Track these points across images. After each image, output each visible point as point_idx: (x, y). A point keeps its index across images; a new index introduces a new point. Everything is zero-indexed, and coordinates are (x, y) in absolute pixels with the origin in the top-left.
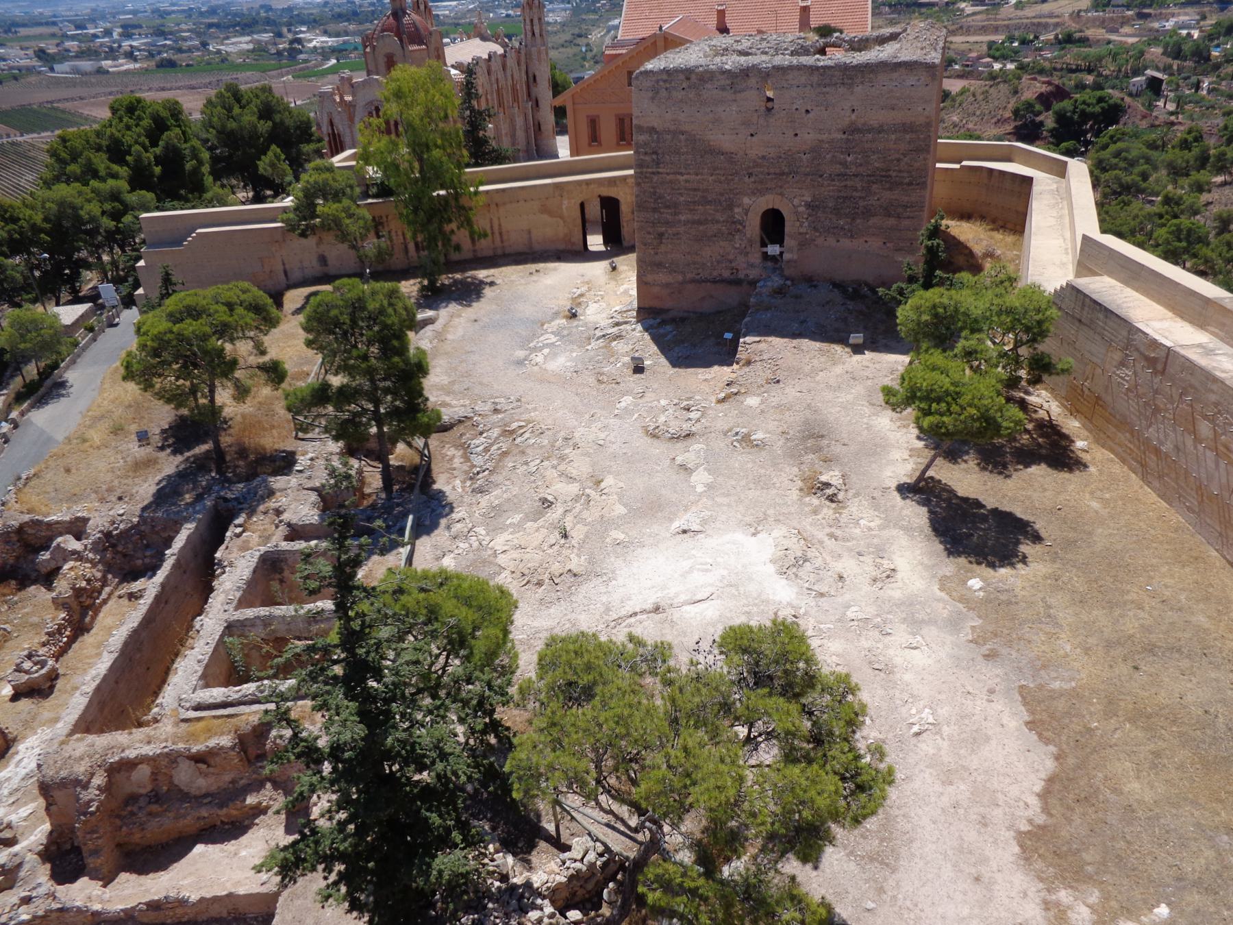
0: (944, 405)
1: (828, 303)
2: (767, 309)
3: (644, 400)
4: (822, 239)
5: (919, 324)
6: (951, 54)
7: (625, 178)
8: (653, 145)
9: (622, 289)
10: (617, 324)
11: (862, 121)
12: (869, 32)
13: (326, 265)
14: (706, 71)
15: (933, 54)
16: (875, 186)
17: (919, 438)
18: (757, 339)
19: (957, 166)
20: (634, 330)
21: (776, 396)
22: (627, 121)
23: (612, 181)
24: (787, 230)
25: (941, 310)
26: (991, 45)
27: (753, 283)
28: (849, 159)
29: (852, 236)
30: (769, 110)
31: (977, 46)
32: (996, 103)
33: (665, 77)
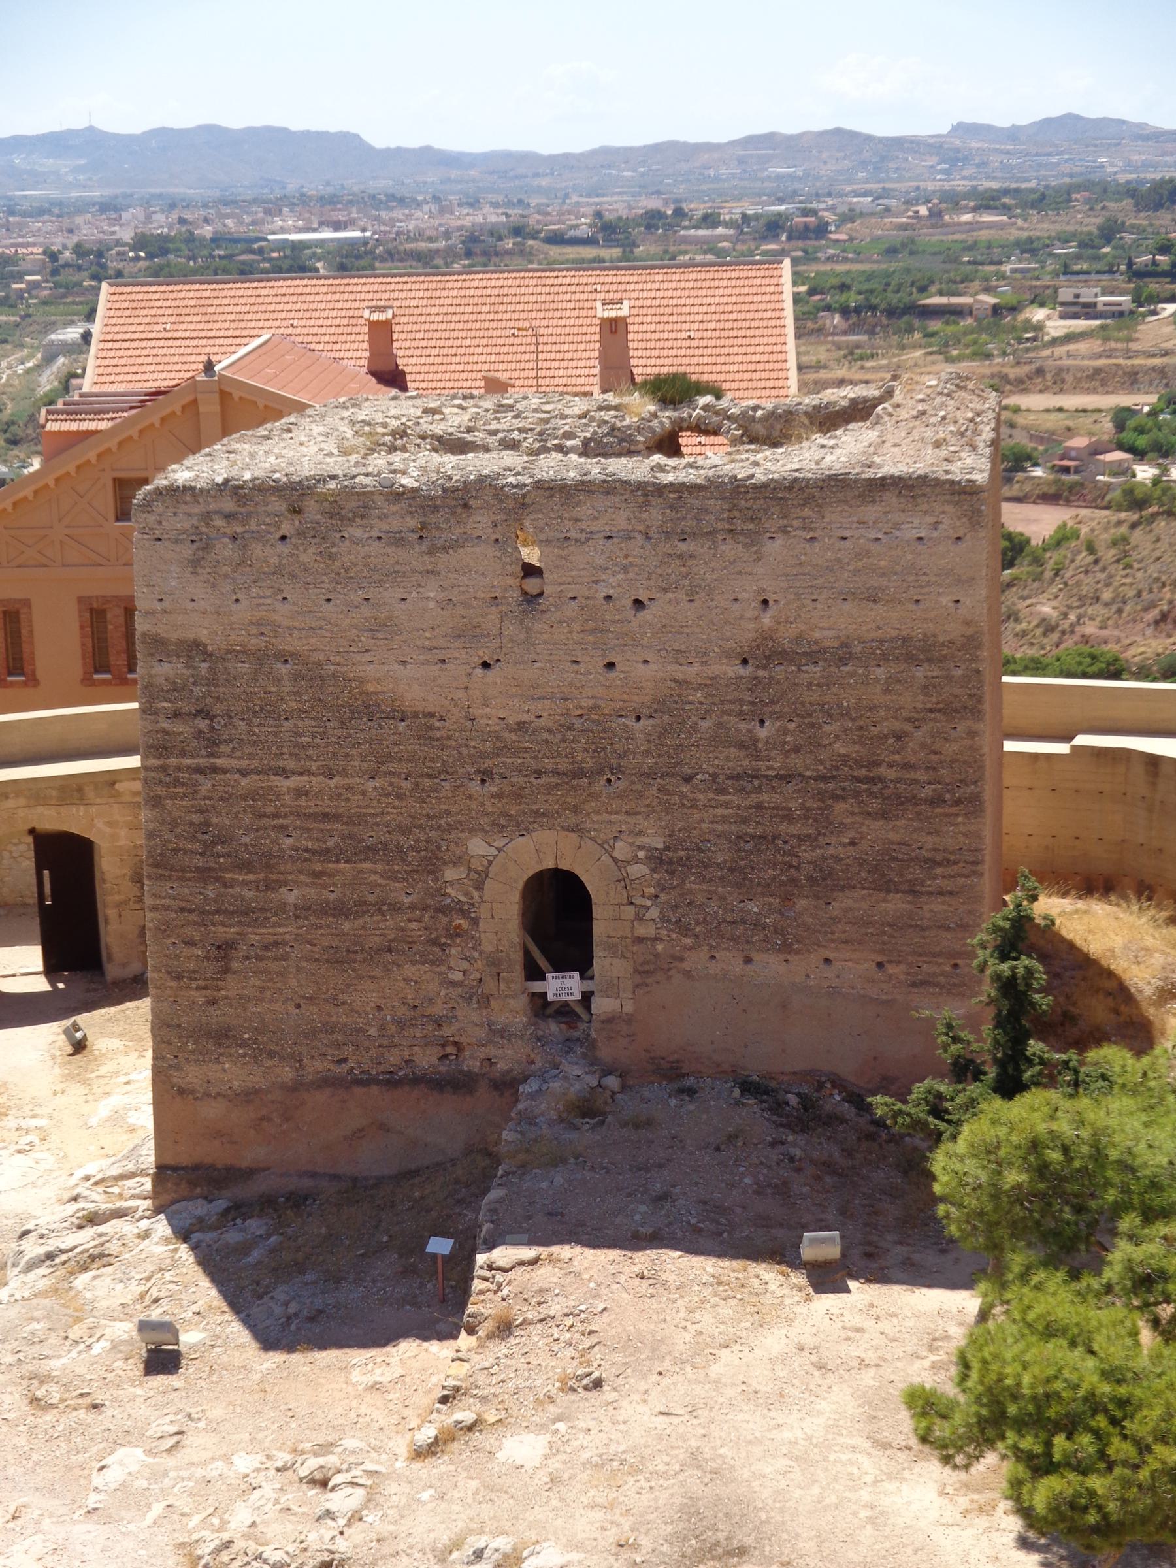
0: (1085, 1439)
1: (731, 1138)
2: (558, 1160)
3: (182, 1456)
4: (704, 954)
5: (996, 1194)
6: (1021, 440)
7: (112, 778)
8: (198, 690)
9: (104, 1109)
10: (93, 1219)
11: (793, 630)
12: (791, 391)
14: (349, 492)
15: (969, 459)
16: (840, 807)
17: (1024, 1543)
18: (528, 1253)
19: (1062, 748)
20: (145, 1235)
21: (596, 1428)
22: (114, 616)
23: (72, 790)
24: (599, 929)
25: (1055, 1156)
26: (1122, 417)
27: (507, 1085)
28: (762, 733)
29: (786, 948)
30: (531, 599)
31: (1086, 421)
32: (1153, 570)
33: (229, 505)
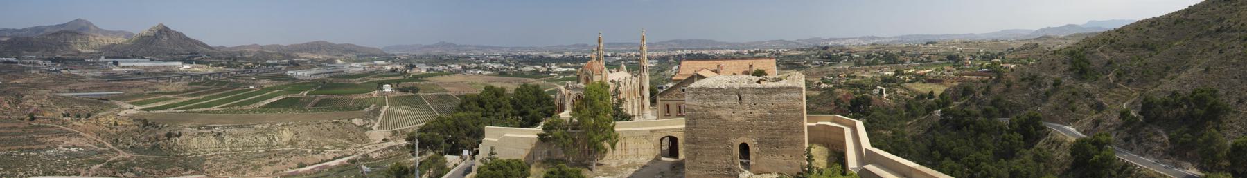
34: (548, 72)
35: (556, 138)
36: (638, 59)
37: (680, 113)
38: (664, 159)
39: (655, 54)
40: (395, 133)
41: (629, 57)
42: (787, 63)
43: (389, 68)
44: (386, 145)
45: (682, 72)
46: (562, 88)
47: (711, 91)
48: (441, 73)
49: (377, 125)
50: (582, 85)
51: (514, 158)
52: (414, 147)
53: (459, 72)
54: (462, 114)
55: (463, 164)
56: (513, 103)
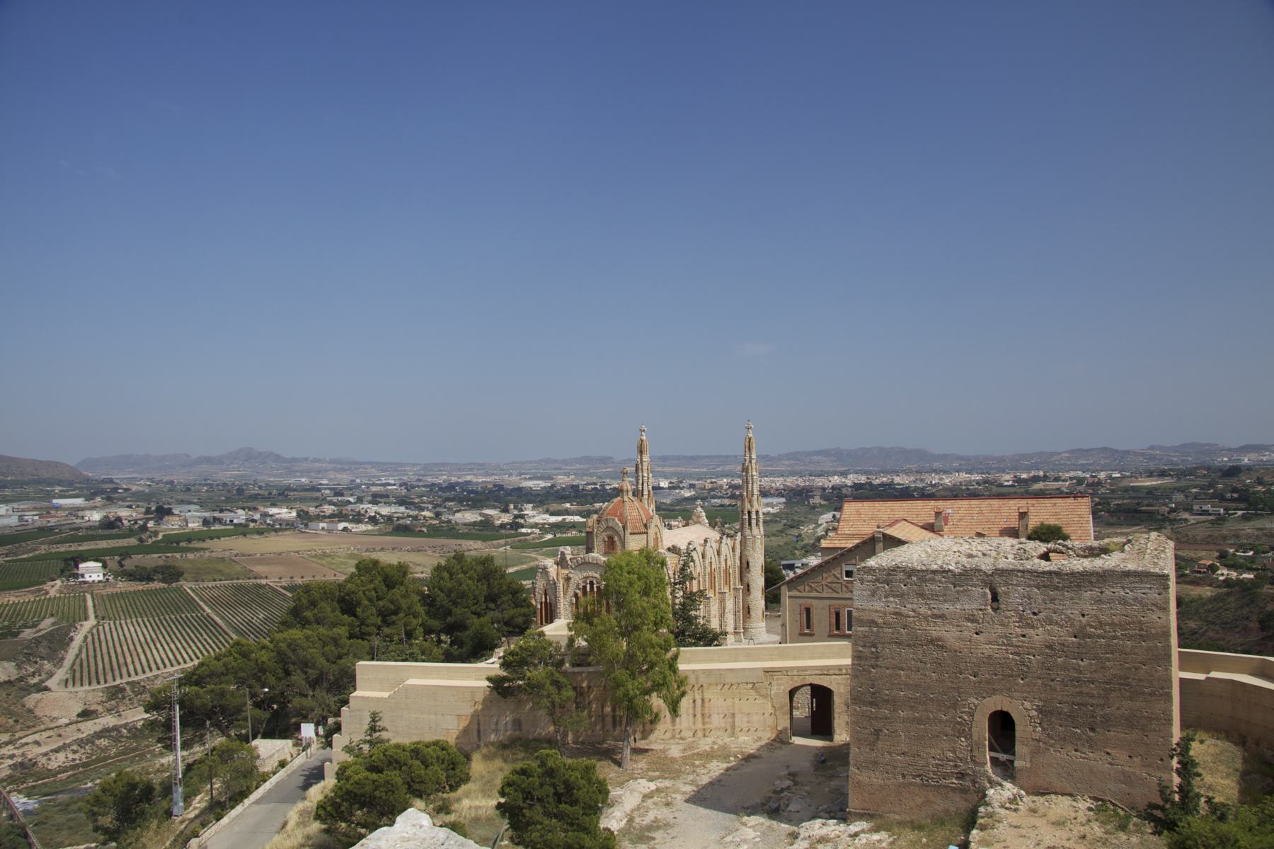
7: (840, 668)
13: (520, 730)
24: (1018, 734)
34: (515, 526)
35: (534, 688)
36: (737, 493)
37: (839, 626)
38: (798, 741)
39: (778, 483)
40: (115, 693)
41: (713, 491)
42: (1120, 510)
43: (96, 516)
44: (90, 727)
45: (845, 528)
46: (550, 563)
47: (919, 578)
48: (242, 530)
49: (61, 674)
50: (598, 556)
51: (429, 738)
52: (168, 726)
53: (288, 526)
54: (296, 633)
55: (300, 760)
56: (429, 601)
